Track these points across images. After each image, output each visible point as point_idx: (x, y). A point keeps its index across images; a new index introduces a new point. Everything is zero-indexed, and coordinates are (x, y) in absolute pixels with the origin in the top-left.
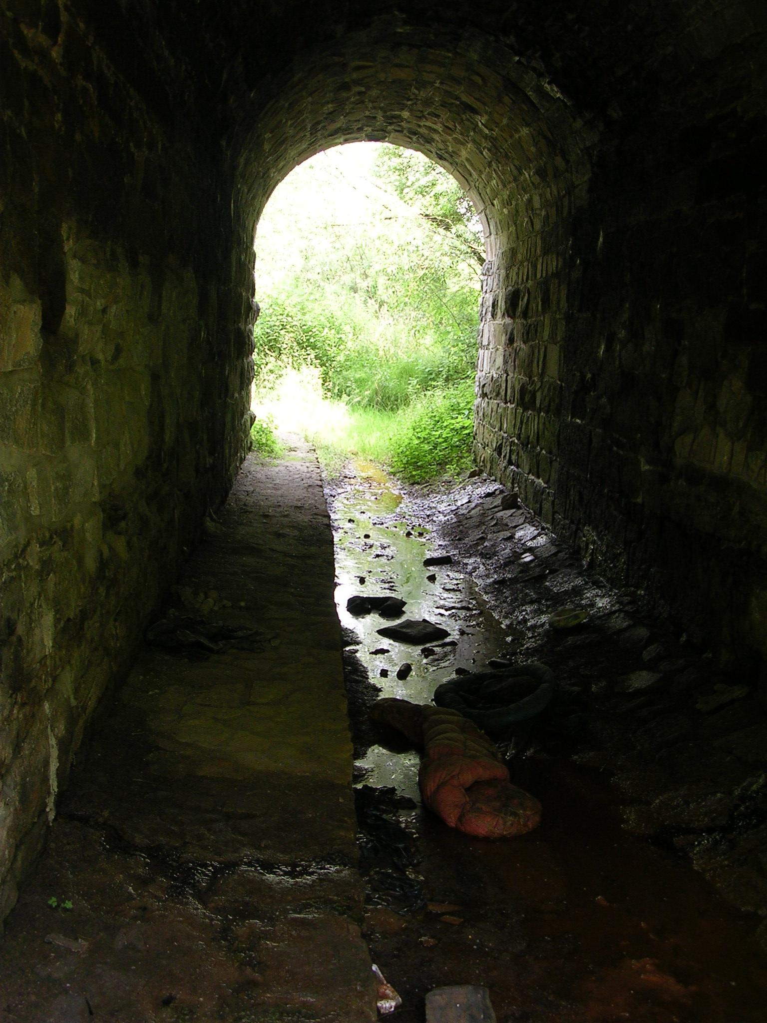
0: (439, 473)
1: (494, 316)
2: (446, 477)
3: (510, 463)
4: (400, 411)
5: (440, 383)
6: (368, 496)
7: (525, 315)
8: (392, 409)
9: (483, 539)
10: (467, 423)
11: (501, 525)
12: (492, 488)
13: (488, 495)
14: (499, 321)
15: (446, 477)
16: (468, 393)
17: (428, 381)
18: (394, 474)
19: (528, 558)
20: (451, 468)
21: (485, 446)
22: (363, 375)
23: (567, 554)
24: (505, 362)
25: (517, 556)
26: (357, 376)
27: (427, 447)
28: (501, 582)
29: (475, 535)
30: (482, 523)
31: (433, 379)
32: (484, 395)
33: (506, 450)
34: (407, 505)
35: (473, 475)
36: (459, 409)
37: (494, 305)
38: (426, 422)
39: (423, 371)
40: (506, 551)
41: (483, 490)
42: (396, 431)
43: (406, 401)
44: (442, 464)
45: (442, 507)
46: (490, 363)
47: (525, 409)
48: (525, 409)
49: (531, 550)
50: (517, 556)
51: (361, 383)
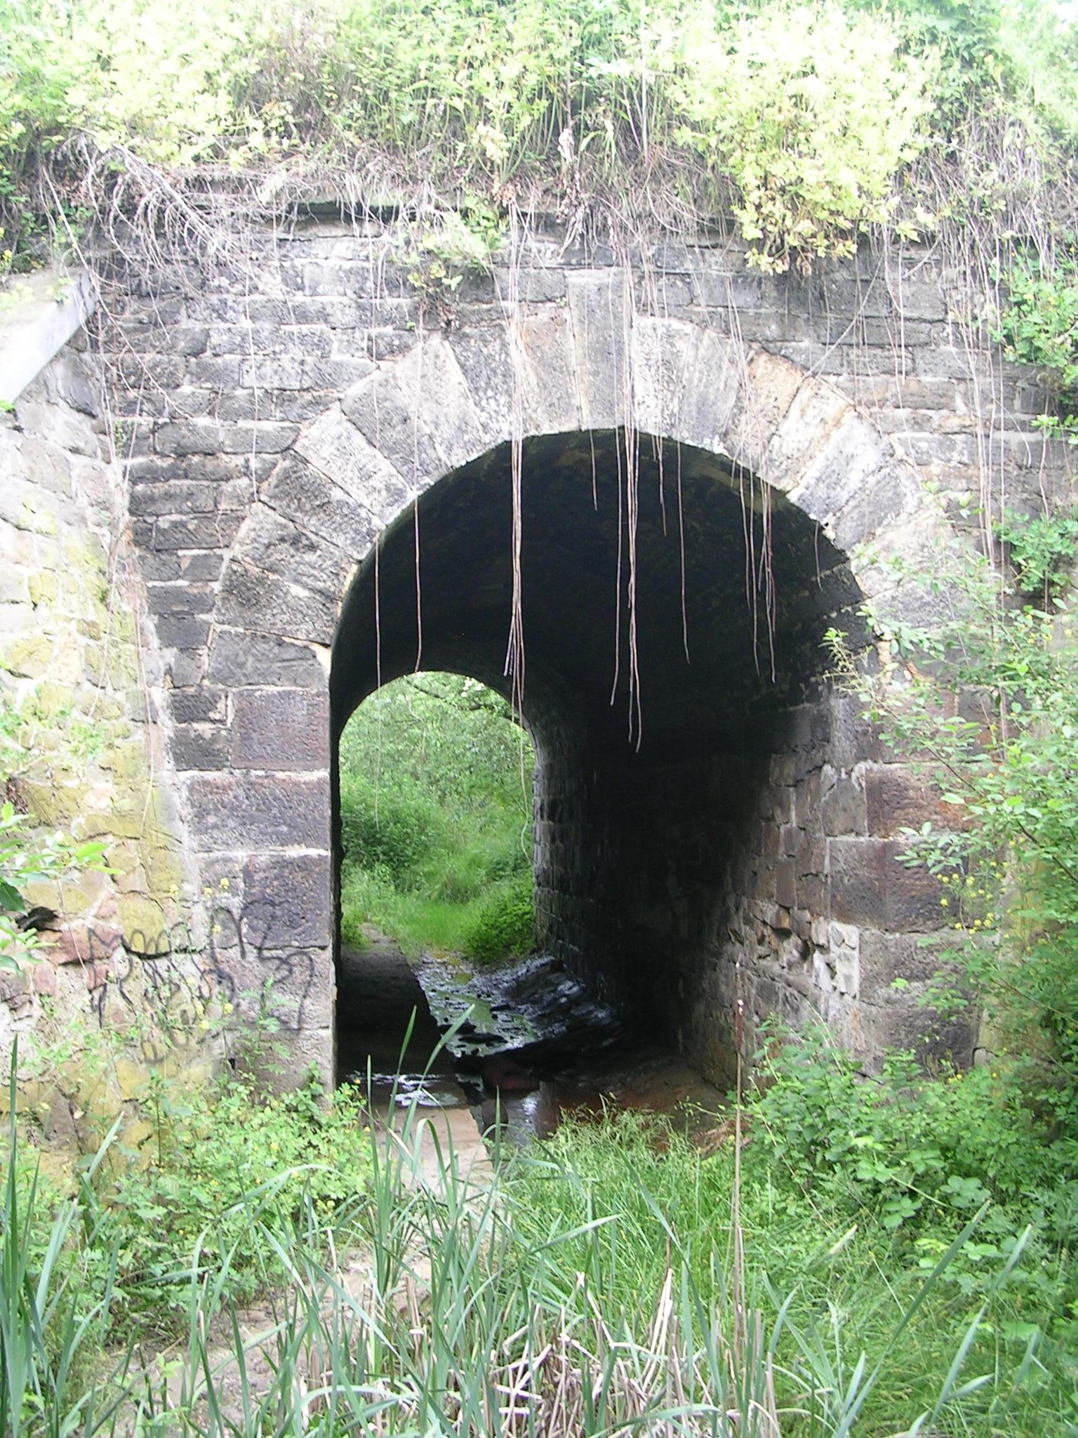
0: (505, 954)
1: (542, 817)
2: (511, 956)
3: (558, 938)
4: (470, 903)
5: (508, 871)
6: (445, 975)
7: (560, 821)
8: (462, 901)
9: (533, 994)
10: (527, 908)
11: (548, 983)
12: (545, 960)
13: (542, 965)
14: (545, 822)
15: (511, 956)
16: (528, 883)
17: (496, 871)
18: (467, 959)
19: (563, 1000)
20: (515, 949)
21: (542, 927)
22: (432, 868)
23: (590, 994)
24: (551, 856)
25: (556, 1000)
26: (426, 870)
27: (494, 932)
28: (543, 1016)
29: (527, 993)
30: (534, 984)
31: (502, 869)
32: (539, 885)
33: (555, 928)
34: (477, 980)
35: (533, 952)
36: (519, 895)
37: (541, 808)
38: (493, 910)
39: (491, 862)
40: (548, 998)
41: (538, 962)
42: (469, 919)
43: (476, 893)
44: (507, 947)
45: (506, 978)
46: (540, 859)
47: (565, 894)
48: (565, 894)
49: (566, 996)
50: (556, 1000)
51: (429, 875)
